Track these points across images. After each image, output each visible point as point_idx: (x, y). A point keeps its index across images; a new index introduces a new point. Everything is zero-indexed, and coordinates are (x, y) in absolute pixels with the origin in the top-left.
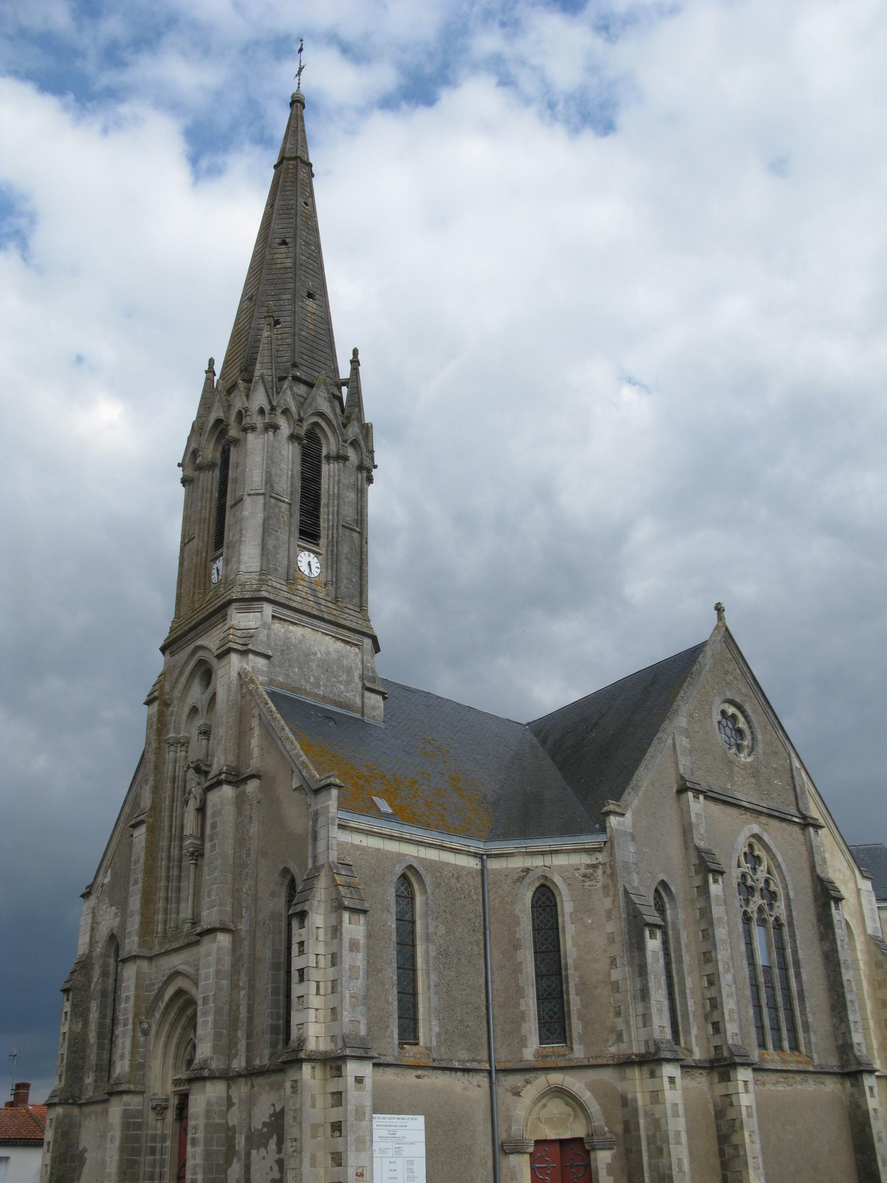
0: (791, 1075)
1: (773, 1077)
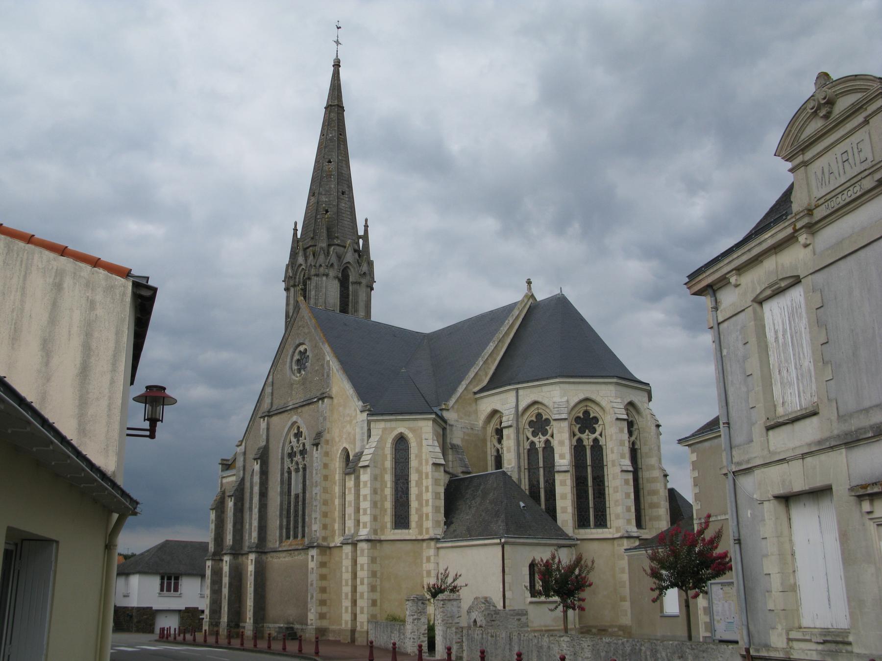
1: (284, 554)
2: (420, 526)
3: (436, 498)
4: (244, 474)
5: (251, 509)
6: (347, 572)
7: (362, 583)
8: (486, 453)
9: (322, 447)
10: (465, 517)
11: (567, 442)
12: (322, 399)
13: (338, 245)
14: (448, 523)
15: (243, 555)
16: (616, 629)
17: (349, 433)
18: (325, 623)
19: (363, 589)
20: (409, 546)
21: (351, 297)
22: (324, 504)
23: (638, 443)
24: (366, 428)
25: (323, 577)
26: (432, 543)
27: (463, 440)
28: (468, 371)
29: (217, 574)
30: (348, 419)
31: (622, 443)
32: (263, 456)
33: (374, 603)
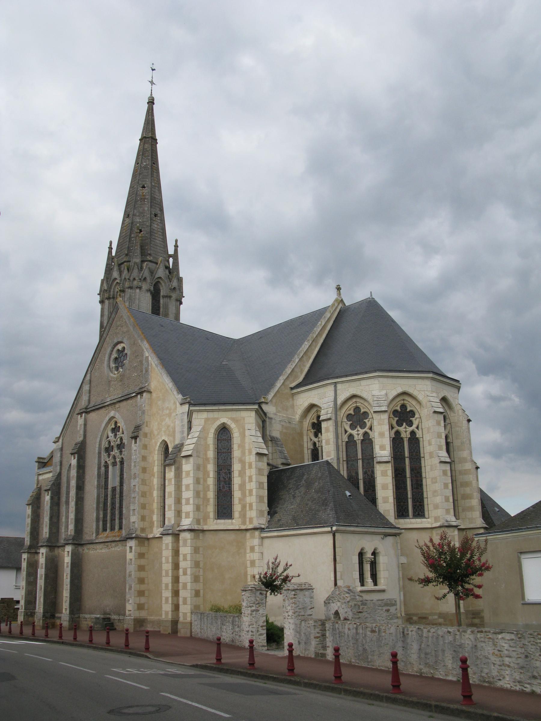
0: (109, 544)
1: (101, 546)
2: (243, 515)
3: (260, 488)
4: (61, 469)
5: (67, 503)
6: (168, 562)
7: (185, 573)
8: (302, 446)
9: (140, 440)
10: (289, 506)
11: (387, 434)
12: (141, 393)
13: (150, 261)
14: (272, 512)
15: (59, 547)
16: (436, 617)
17: (168, 426)
18: (143, 614)
19: (185, 579)
20: (232, 536)
21: (161, 310)
22: (142, 496)
23: (450, 436)
24: (186, 420)
25: (141, 568)
26: (257, 533)
27: (281, 433)
28: (285, 367)
29: (33, 566)
30: (168, 412)
31: (439, 436)
32: (80, 451)
33: (197, 593)
